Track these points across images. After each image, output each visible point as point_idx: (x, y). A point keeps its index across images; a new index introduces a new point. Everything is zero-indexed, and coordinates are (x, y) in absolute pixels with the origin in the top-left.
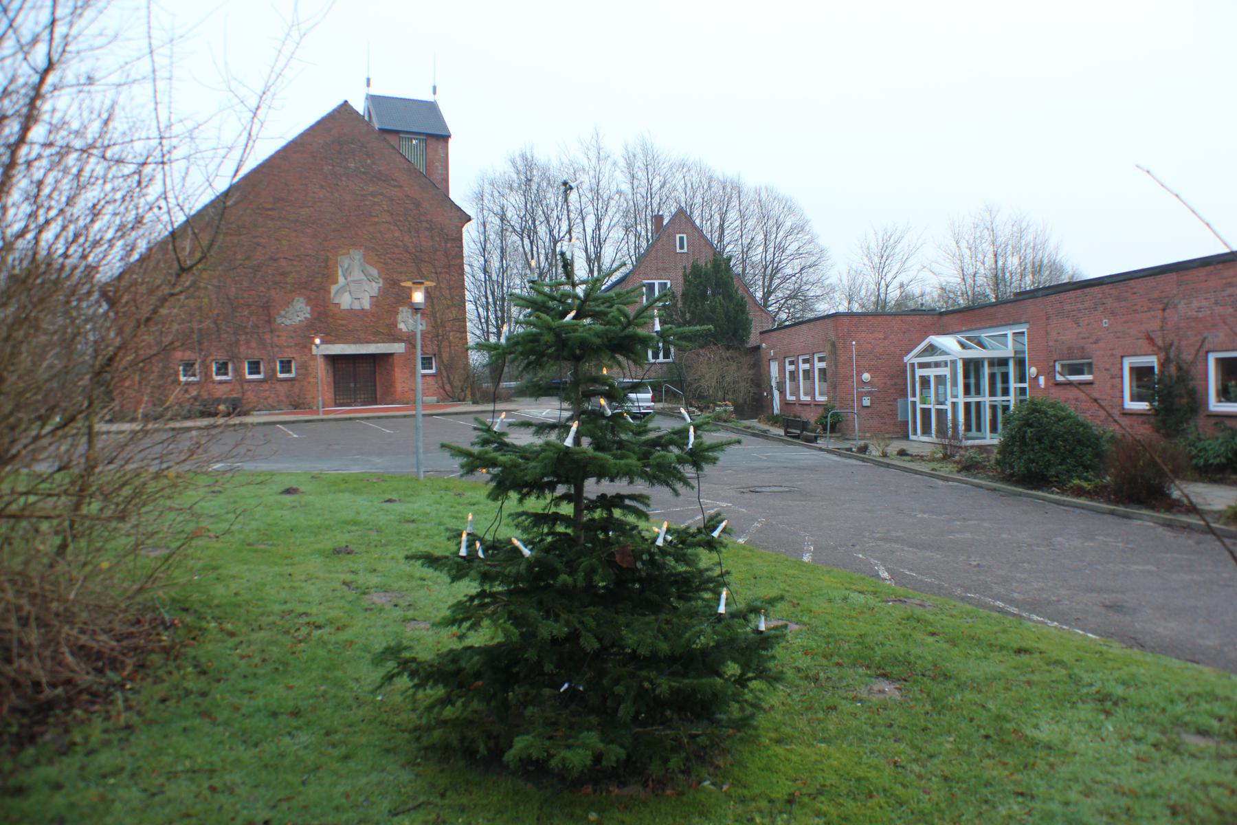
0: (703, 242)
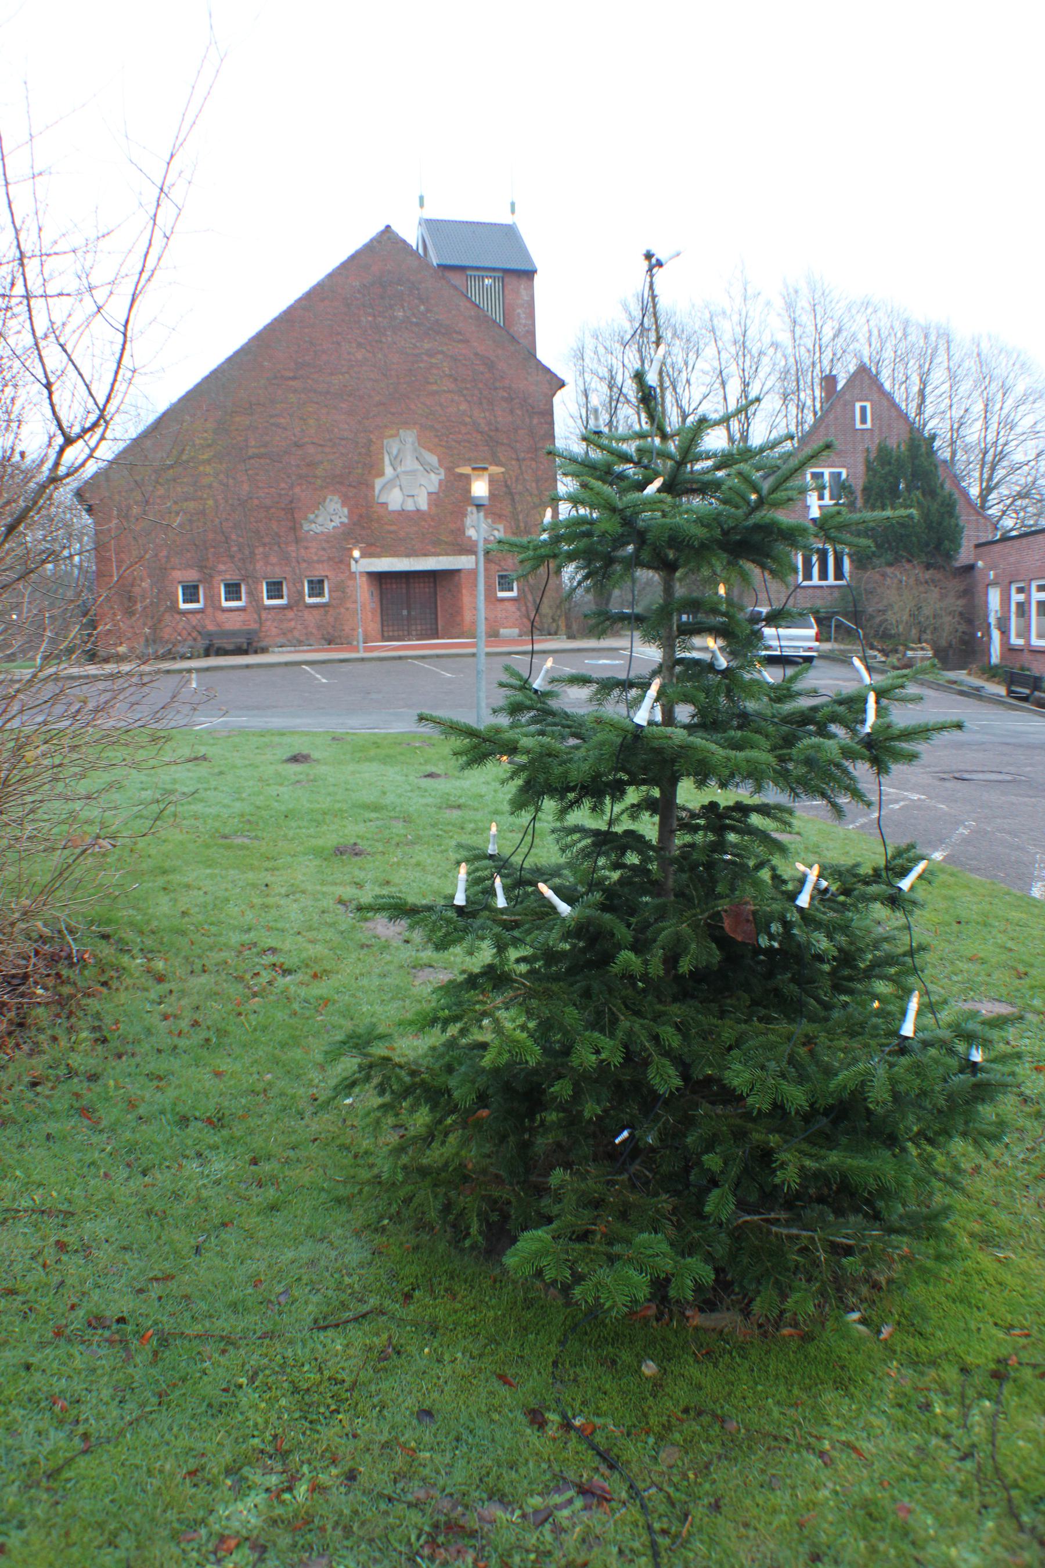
0: (894, 413)
